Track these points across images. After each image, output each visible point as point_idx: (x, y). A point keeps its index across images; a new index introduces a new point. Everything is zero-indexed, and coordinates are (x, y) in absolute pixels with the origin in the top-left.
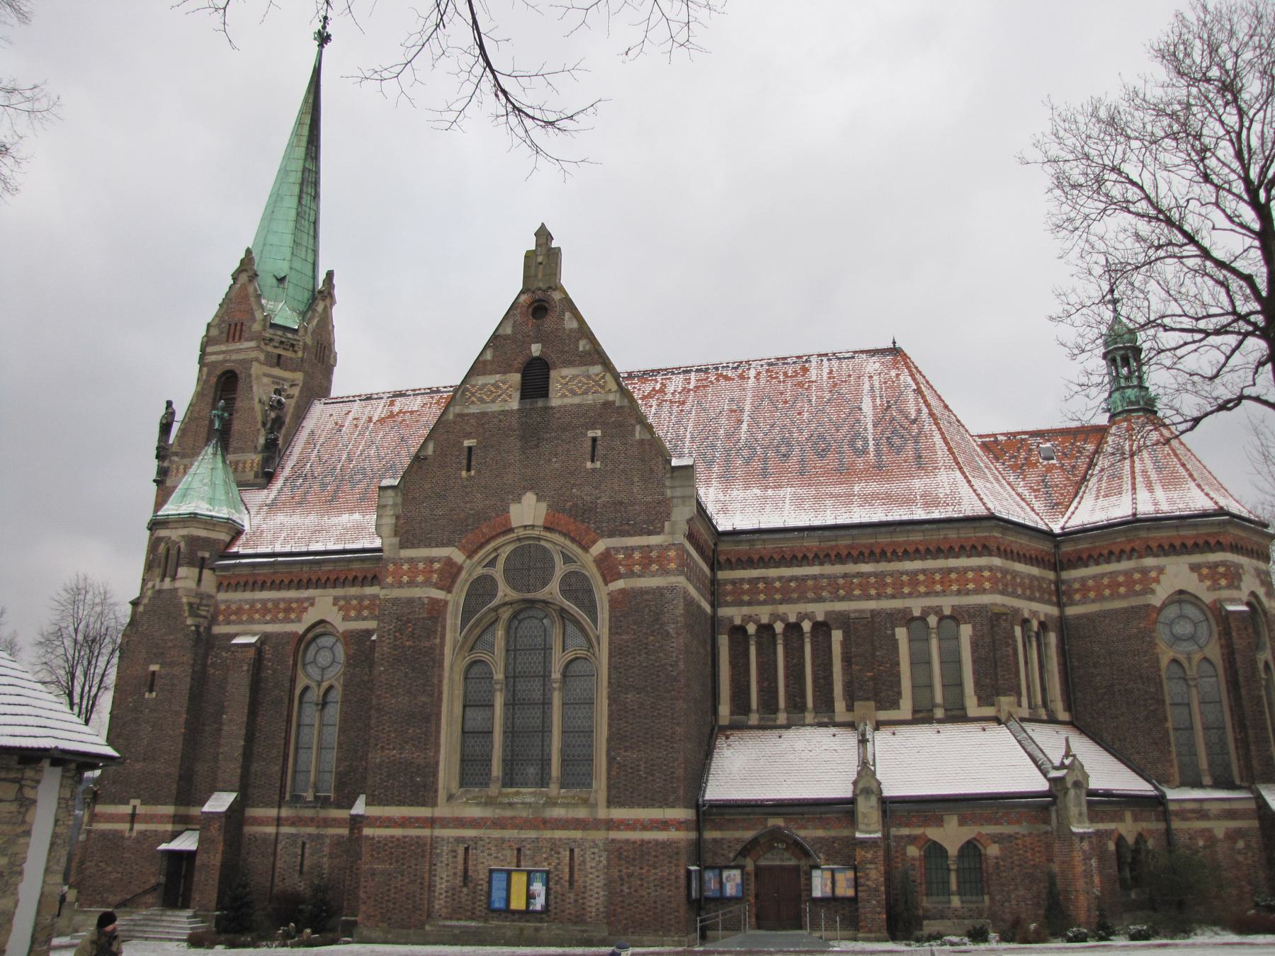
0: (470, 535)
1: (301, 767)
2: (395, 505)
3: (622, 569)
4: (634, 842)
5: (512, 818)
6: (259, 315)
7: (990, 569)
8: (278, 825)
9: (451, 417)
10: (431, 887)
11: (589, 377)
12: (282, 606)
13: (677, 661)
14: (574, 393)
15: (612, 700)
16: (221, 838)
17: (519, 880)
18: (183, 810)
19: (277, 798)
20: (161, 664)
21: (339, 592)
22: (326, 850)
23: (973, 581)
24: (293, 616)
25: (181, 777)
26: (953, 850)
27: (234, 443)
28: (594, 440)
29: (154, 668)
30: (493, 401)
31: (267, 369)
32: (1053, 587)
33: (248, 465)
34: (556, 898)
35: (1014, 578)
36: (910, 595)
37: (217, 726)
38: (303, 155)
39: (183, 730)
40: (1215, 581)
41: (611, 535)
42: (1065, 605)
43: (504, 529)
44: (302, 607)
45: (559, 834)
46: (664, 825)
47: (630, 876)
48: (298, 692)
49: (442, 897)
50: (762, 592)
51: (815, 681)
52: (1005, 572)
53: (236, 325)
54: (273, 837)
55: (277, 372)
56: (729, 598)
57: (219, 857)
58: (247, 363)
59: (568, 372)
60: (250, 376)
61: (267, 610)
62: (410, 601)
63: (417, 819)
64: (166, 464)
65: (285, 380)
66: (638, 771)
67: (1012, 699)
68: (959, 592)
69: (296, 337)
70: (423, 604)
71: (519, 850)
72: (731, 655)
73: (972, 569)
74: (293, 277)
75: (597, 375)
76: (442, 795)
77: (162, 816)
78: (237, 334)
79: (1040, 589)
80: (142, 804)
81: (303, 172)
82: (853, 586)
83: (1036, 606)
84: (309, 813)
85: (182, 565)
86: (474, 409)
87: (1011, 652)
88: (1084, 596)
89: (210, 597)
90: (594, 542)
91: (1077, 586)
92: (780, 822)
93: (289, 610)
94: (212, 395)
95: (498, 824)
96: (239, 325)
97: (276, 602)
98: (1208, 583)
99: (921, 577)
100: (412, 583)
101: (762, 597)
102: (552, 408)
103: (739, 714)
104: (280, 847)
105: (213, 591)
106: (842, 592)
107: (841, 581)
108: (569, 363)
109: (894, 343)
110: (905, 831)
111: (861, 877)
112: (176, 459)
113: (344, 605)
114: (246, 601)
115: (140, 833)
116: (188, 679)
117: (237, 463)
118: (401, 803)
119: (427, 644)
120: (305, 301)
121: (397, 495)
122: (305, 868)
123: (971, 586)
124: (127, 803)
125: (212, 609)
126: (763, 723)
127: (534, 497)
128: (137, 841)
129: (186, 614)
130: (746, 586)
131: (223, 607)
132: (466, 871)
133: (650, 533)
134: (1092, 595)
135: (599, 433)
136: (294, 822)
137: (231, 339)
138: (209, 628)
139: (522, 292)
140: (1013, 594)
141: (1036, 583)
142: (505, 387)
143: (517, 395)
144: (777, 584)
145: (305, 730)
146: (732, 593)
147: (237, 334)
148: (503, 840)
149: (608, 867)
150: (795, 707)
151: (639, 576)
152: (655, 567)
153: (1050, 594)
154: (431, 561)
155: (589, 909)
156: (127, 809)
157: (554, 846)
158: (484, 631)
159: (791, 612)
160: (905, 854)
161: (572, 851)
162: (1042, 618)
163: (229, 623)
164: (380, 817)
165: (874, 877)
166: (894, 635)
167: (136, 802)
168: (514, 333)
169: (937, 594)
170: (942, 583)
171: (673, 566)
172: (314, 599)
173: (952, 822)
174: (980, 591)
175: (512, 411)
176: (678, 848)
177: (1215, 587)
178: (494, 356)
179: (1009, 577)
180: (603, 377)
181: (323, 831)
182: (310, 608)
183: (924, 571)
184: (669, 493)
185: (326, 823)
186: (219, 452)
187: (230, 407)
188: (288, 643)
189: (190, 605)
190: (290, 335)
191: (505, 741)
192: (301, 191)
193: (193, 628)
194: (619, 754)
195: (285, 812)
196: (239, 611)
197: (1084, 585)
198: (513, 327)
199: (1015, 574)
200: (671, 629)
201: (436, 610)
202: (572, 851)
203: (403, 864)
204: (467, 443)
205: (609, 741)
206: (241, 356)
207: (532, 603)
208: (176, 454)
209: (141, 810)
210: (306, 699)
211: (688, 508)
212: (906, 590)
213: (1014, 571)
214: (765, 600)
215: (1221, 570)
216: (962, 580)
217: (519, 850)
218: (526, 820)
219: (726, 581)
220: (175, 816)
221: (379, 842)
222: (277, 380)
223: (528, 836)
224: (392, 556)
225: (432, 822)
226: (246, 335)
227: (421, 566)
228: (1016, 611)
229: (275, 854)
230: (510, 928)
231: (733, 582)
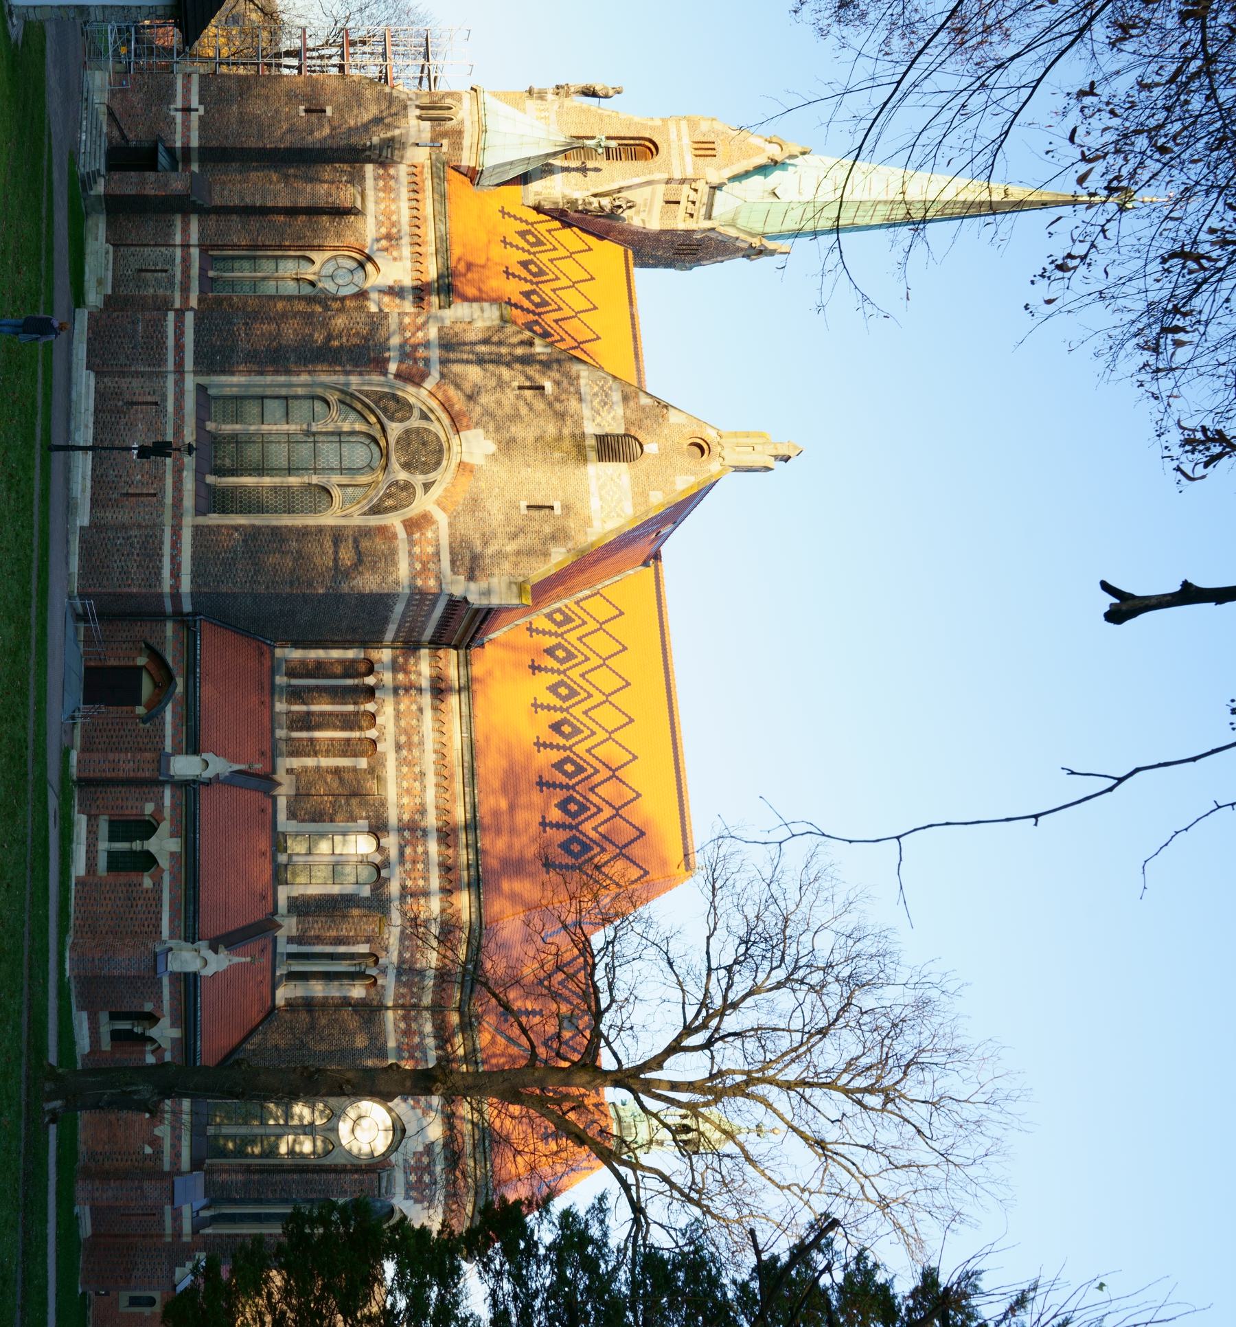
1: (237, 265)
8: (182, 246)
18: (194, 155)
22: (161, 292)
25: (225, 149)
46: (176, 574)
47: (132, 545)
48: (308, 254)
54: (171, 242)
57: (153, 192)
63: (182, 359)
64: (550, 97)
74: (778, 208)
76: (203, 380)
77: (189, 137)
92: (180, 688)
104: (163, 249)
110: (167, 801)
115: (174, 118)
118: (197, 343)
119: (344, 359)
122: (143, 274)
124: (200, 103)
128: (167, 116)
129: (382, 136)
138: (370, 161)
143: (599, 432)
145: (272, 264)
150: (292, 721)
151: (410, 552)
156: (195, 103)
158: (359, 412)
160: (147, 800)
161: (155, 495)
167: (201, 111)
173: (176, 1033)
180: (618, 515)
207: (386, 455)
209: (194, 116)
210: (302, 262)
229: (156, 245)
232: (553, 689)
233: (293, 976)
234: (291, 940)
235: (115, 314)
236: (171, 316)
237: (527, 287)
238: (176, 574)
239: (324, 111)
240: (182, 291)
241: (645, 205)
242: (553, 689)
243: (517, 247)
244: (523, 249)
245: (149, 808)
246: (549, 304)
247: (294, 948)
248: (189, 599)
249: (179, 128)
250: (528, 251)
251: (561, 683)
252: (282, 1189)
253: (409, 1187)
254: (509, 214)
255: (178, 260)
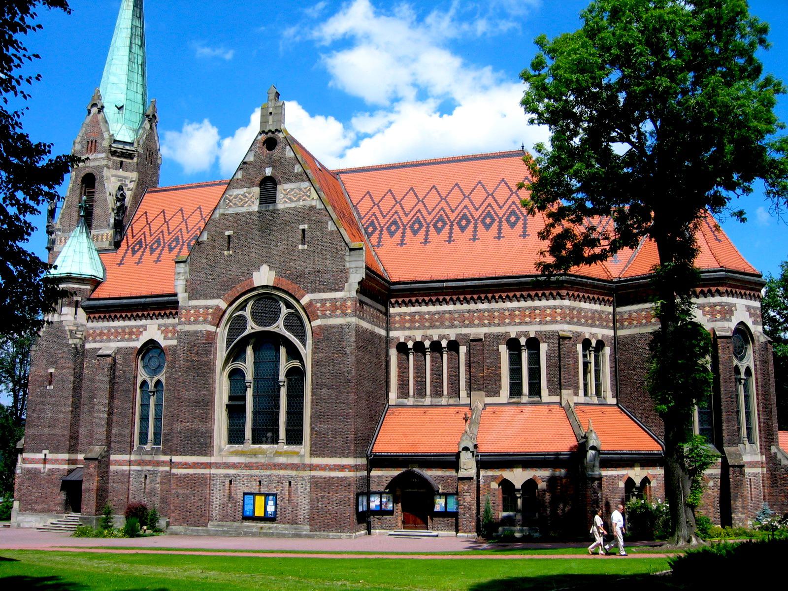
0: (230, 292)
2: (185, 272)
3: (319, 313)
4: (325, 478)
5: (256, 463)
6: (106, 135)
7: (561, 308)
9: (217, 216)
10: (210, 503)
11: (300, 190)
12: (127, 330)
13: (351, 370)
14: (291, 200)
15: (313, 394)
16: (96, 473)
17: (260, 500)
18: (73, 456)
19: (128, 449)
20: (56, 368)
21: (160, 321)
22: (159, 480)
23: (550, 315)
24: (134, 337)
26: (518, 486)
27: (95, 223)
28: (303, 230)
29: (52, 370)
30: (242, 206)
31: (113, 172)
32: (611, 317)
33: (105, 237)
34: (281, 510)
35: (579, 312)
36: (509, 324)
37: (91, 405)
38: (131, 16)
39: (71, 409)
40: (713, 316)
41: (313, 292)
42: (618, 329)
43: (250, 288)
44: (139, 331)
45: (281, 473)
46: (342, 468)
49: (217, 508)
50: (417, 321)
51: (449, 378)
52: (572, 309)
53: (92, 141)
54: (128, 472)
55: (121, 172)
56: (397, 325)
57: (95, 484)
58: (100, 168)
59: (288, 186)
60: (103, 177)
61: (119, 334)
62: (196, 332)
63: (202, 464)
65: (126, 178)
66: (328, 436)
67: (571, 392)
68: (540, 323)
69: (132, 148)
70: (203, 335)
71: (260, 482)
72: (398, 361)
73: (550, 308)
74: (128, 106)
75: (306, 188)
78: (93, 148)
79: (600, 318)
80: (49, 453)
81: (132, 28)
82: (474, 318)
83: (594, 330)
84: (148, 458)
85: (65, 306)
86: (231, 211)
87: (572, 362)
88: (630, 323)
89: (83, 325)
90: (303, 296)
91: (626, 316)
93: (133, 333)
94: (79, 190)
95: (248, 466)
96: (94, 142)
97: (123, 328)
98: (709, 317)
99: (517, 313)
100: (196, 322)
101: (417, 325)
102: (278, 210)
103: (402, 398)
105: (85, 322)
106: (467, 322)
107: (466, 315)
108: (288, 181)
109: (523, 147)
111: (460, 500)
112: (59, 233)
113: (164, 330)
114: (105, 328)
115: (50, 470)
116: (72, 377)
117: (98, 236)
119: (206, 359)
120: (138, 122)
121: (186, 266)
122: (147, 491)
123: (548, 319)
124: (41, 452)
125: (84, 334)
126: (416, 404)
127: (268, 268)
129: (69, 337)
130: (408, 318)
131: (91, 332)
132: (230, 494)
133: (336, 290)
134: (635, 322)
135: (306, 227)
136: (140, 463)
137: (89, 152)
138: (83, 346)
139: (260, 134)
140: (579, 323)
141: (597, 315)
142: (249, 197)
143: (257, 202)
144: (427, 317)
146: (399, 322)
147: (93, 148)
148: (251, 476)
149: (310, 492)
150: (437, 393)
151: (330, 317)
152: (339, 312)
153: (608, 322)
154: (207, 308)
155: (300, 517)
156: (42, 456)
157: (280, 480)
159: (435, 334)
161: (290, 483)
162: (600, 338)
163: (95, 342)
164: (181, 463)
165: (468, 500)
166: (498, 350)
167: (46, 452)
168: (255, 160)
169: (526, 323)
170: (530, 316)
171: (349, 311)
172: (146, 326)
174: (554, 322)
175: (254, 212)
176: (349, 482)
177: (713, 319)
178: (243, 176)
179: (575, 312)
181: (156, 468)
182: (144, 332)
183: (519, 309)
184: (348, 265)
185: (158, 464)
186: (84, 231)
187: (91, 195)
188: (132, 353)
189: (71, 331)
190: (128, 147)
191: (746, 280)
192: (131, 43)
193: (73, 346)
194: (316, 426)
195: (133, 457)
196: (101, 334)
197: (630, 316)
198: (255, 156)
199: (580, 310)
200: (347, 350)
201: (211, 338)
202: (290, 483)
203: (194, 490)
204: (227, 233)
205: (311, 417)
206: (97, 163)
208: (59, 230)
211: (359, 275)
212: (507, 321)
213: (580, 308)
214: (419, 327)
215: (718, 308)
216: (543, 315)
217: (260, 482)
218: (263, 464)
219: (396, 314)
220: (69, 460)
221: (180, 477)
222: (121, 178)
223: (265, 474)
224: (184, 305)
225: (208, 465)
226: (98, 149)
227: (201, 311)
228: (579, 335)
229: (129, 482)
230: (254, 526)
231: (400, 315)
232: (415, 232)
233: (598, 393)
234: (576, 394)
235: (172, 508)
236: (174, 471)
237: (166, 249)
238: (342, 468)
239: (51, 373)
240: (158, 465)
241: (122, 181)
242: (415, 232)
243: (142, 255)
244: (143, 252)
245: (494, 485)
246: (441, 215)
247: (581, 392)
248: (75, 458)
249: (56, 466)
250: (144, 249)
251: (411, 228)
252: (730, 397)
253: (724, 319)
254: (121, 261)
255: (139, 468)
